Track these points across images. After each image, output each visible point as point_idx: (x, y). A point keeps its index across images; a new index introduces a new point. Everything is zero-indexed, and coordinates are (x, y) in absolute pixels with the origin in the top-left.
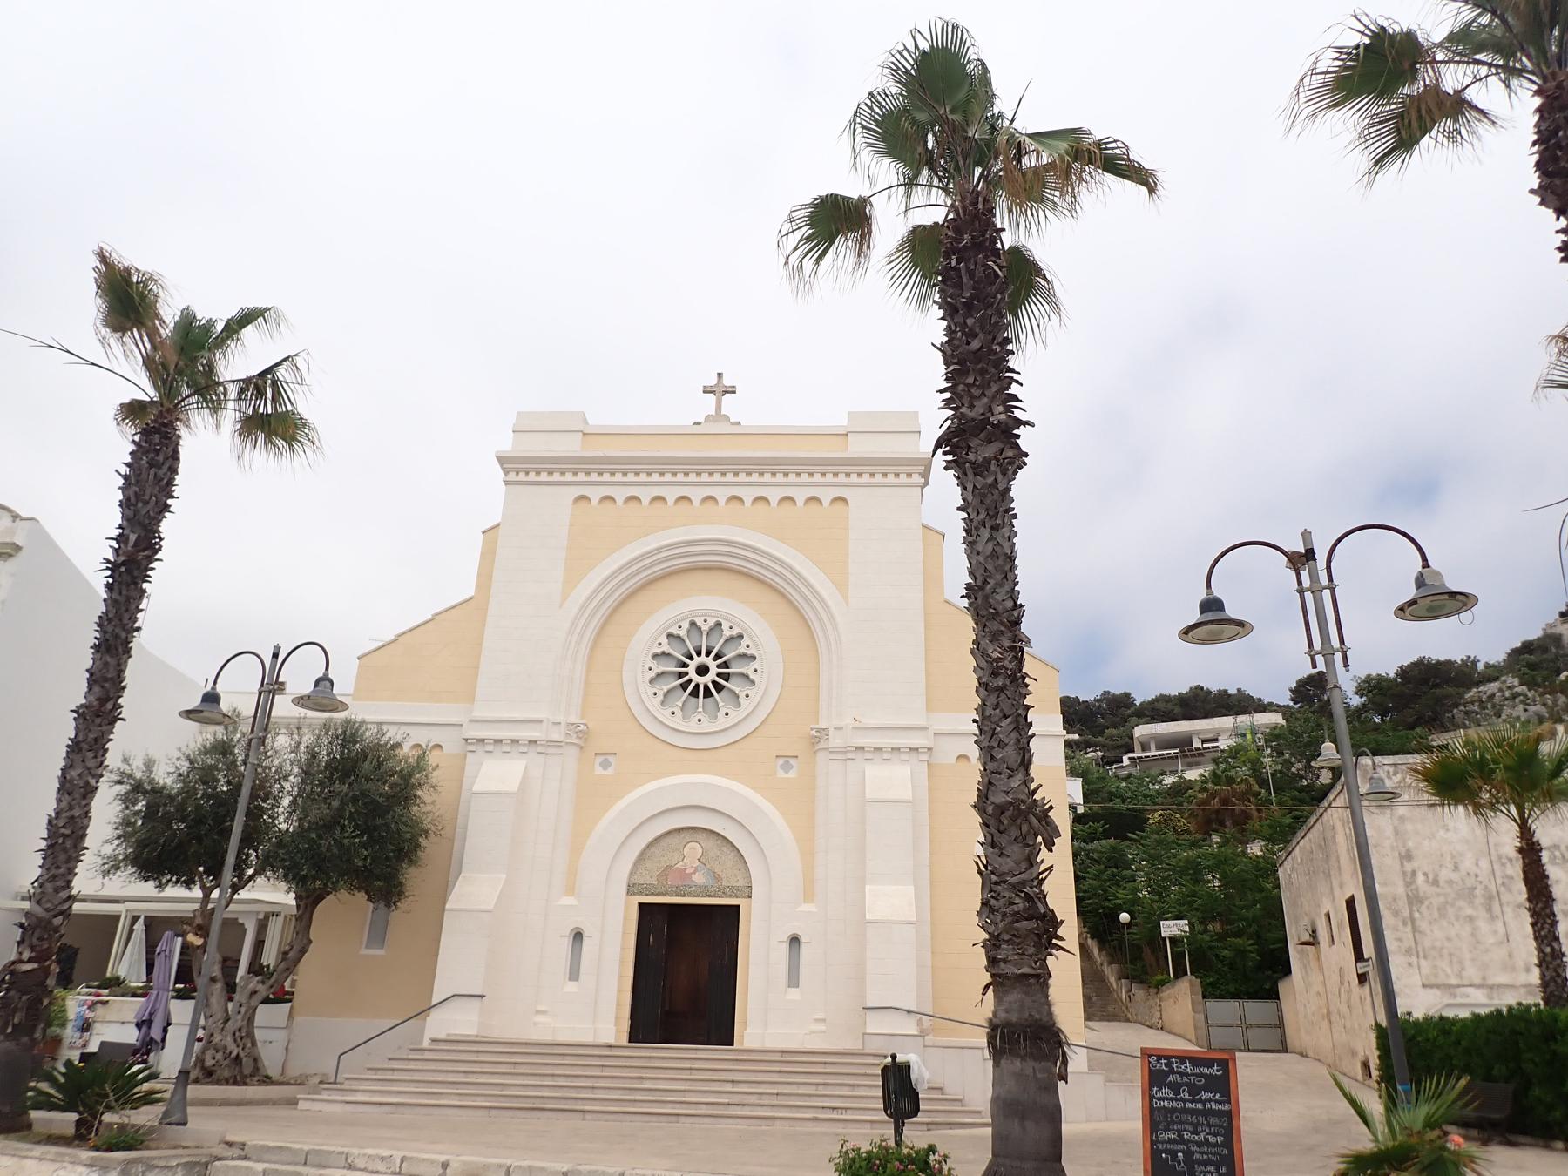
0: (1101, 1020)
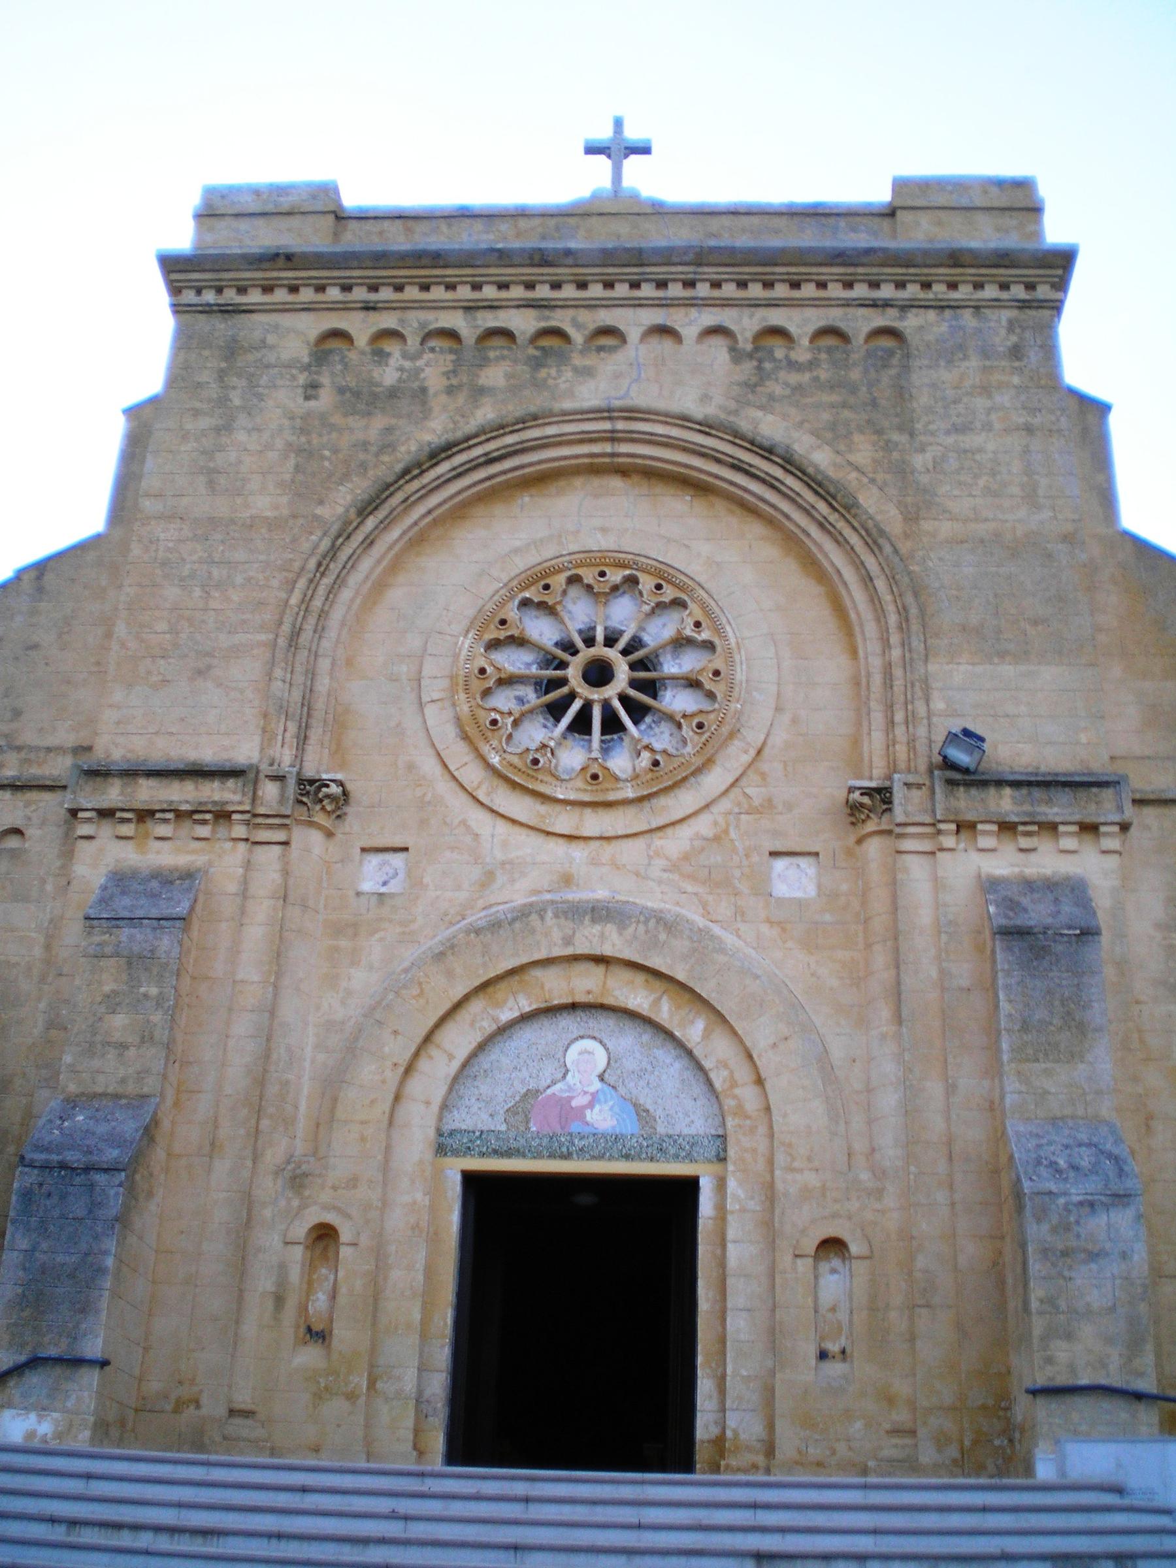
0: (726, 1188)
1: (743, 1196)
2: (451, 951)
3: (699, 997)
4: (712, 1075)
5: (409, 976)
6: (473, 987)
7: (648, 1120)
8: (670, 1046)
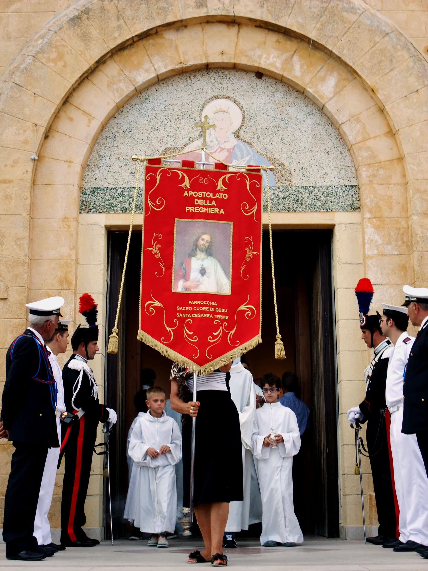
1: (380, 242)
2: (86, 16)
3: (330, 54)
4: (345, 128)
5: (46, 40)
6: (109, 49)
7: (283, 172)
8: (301, 103)
